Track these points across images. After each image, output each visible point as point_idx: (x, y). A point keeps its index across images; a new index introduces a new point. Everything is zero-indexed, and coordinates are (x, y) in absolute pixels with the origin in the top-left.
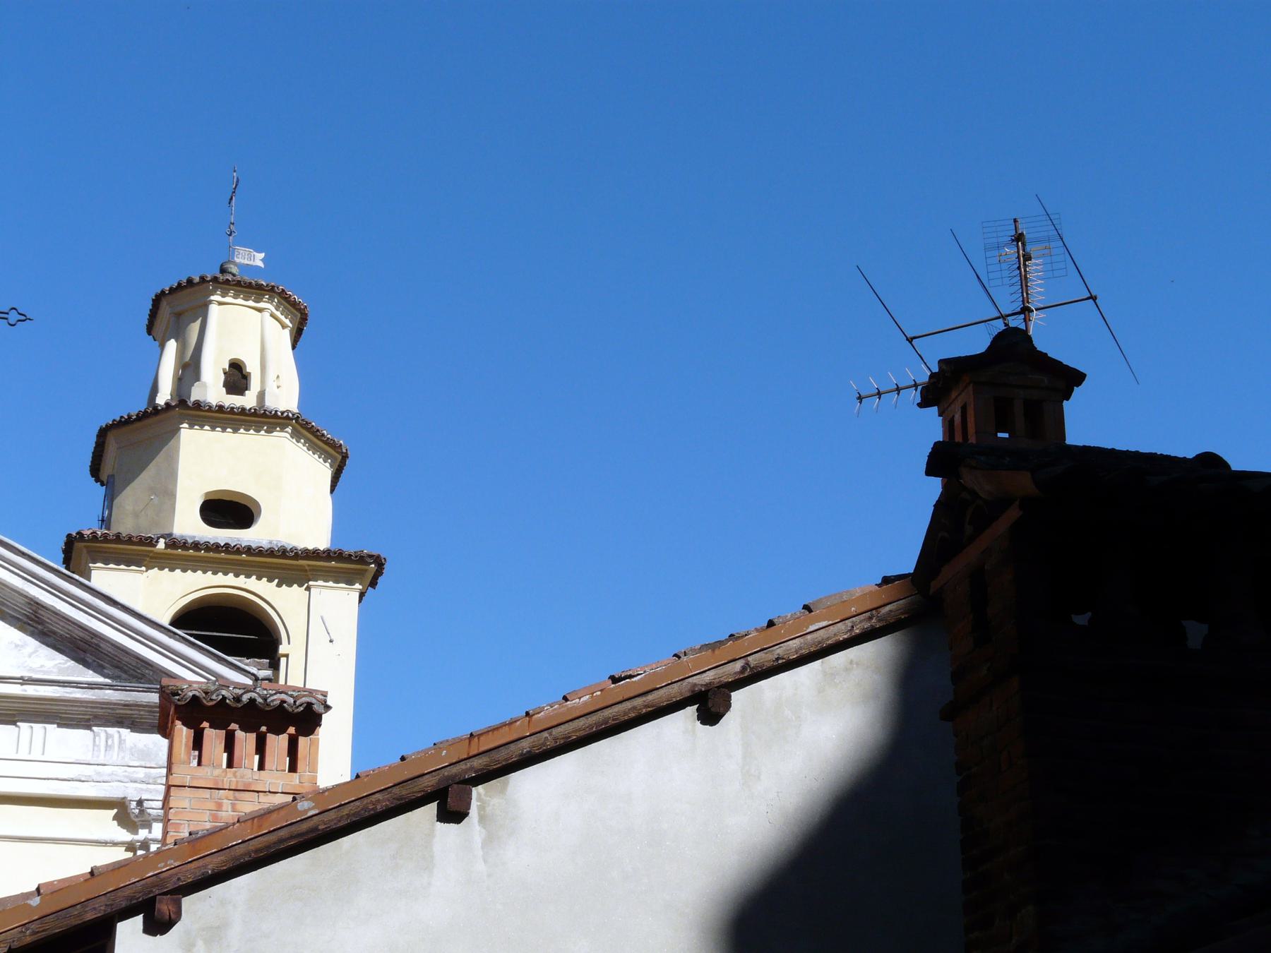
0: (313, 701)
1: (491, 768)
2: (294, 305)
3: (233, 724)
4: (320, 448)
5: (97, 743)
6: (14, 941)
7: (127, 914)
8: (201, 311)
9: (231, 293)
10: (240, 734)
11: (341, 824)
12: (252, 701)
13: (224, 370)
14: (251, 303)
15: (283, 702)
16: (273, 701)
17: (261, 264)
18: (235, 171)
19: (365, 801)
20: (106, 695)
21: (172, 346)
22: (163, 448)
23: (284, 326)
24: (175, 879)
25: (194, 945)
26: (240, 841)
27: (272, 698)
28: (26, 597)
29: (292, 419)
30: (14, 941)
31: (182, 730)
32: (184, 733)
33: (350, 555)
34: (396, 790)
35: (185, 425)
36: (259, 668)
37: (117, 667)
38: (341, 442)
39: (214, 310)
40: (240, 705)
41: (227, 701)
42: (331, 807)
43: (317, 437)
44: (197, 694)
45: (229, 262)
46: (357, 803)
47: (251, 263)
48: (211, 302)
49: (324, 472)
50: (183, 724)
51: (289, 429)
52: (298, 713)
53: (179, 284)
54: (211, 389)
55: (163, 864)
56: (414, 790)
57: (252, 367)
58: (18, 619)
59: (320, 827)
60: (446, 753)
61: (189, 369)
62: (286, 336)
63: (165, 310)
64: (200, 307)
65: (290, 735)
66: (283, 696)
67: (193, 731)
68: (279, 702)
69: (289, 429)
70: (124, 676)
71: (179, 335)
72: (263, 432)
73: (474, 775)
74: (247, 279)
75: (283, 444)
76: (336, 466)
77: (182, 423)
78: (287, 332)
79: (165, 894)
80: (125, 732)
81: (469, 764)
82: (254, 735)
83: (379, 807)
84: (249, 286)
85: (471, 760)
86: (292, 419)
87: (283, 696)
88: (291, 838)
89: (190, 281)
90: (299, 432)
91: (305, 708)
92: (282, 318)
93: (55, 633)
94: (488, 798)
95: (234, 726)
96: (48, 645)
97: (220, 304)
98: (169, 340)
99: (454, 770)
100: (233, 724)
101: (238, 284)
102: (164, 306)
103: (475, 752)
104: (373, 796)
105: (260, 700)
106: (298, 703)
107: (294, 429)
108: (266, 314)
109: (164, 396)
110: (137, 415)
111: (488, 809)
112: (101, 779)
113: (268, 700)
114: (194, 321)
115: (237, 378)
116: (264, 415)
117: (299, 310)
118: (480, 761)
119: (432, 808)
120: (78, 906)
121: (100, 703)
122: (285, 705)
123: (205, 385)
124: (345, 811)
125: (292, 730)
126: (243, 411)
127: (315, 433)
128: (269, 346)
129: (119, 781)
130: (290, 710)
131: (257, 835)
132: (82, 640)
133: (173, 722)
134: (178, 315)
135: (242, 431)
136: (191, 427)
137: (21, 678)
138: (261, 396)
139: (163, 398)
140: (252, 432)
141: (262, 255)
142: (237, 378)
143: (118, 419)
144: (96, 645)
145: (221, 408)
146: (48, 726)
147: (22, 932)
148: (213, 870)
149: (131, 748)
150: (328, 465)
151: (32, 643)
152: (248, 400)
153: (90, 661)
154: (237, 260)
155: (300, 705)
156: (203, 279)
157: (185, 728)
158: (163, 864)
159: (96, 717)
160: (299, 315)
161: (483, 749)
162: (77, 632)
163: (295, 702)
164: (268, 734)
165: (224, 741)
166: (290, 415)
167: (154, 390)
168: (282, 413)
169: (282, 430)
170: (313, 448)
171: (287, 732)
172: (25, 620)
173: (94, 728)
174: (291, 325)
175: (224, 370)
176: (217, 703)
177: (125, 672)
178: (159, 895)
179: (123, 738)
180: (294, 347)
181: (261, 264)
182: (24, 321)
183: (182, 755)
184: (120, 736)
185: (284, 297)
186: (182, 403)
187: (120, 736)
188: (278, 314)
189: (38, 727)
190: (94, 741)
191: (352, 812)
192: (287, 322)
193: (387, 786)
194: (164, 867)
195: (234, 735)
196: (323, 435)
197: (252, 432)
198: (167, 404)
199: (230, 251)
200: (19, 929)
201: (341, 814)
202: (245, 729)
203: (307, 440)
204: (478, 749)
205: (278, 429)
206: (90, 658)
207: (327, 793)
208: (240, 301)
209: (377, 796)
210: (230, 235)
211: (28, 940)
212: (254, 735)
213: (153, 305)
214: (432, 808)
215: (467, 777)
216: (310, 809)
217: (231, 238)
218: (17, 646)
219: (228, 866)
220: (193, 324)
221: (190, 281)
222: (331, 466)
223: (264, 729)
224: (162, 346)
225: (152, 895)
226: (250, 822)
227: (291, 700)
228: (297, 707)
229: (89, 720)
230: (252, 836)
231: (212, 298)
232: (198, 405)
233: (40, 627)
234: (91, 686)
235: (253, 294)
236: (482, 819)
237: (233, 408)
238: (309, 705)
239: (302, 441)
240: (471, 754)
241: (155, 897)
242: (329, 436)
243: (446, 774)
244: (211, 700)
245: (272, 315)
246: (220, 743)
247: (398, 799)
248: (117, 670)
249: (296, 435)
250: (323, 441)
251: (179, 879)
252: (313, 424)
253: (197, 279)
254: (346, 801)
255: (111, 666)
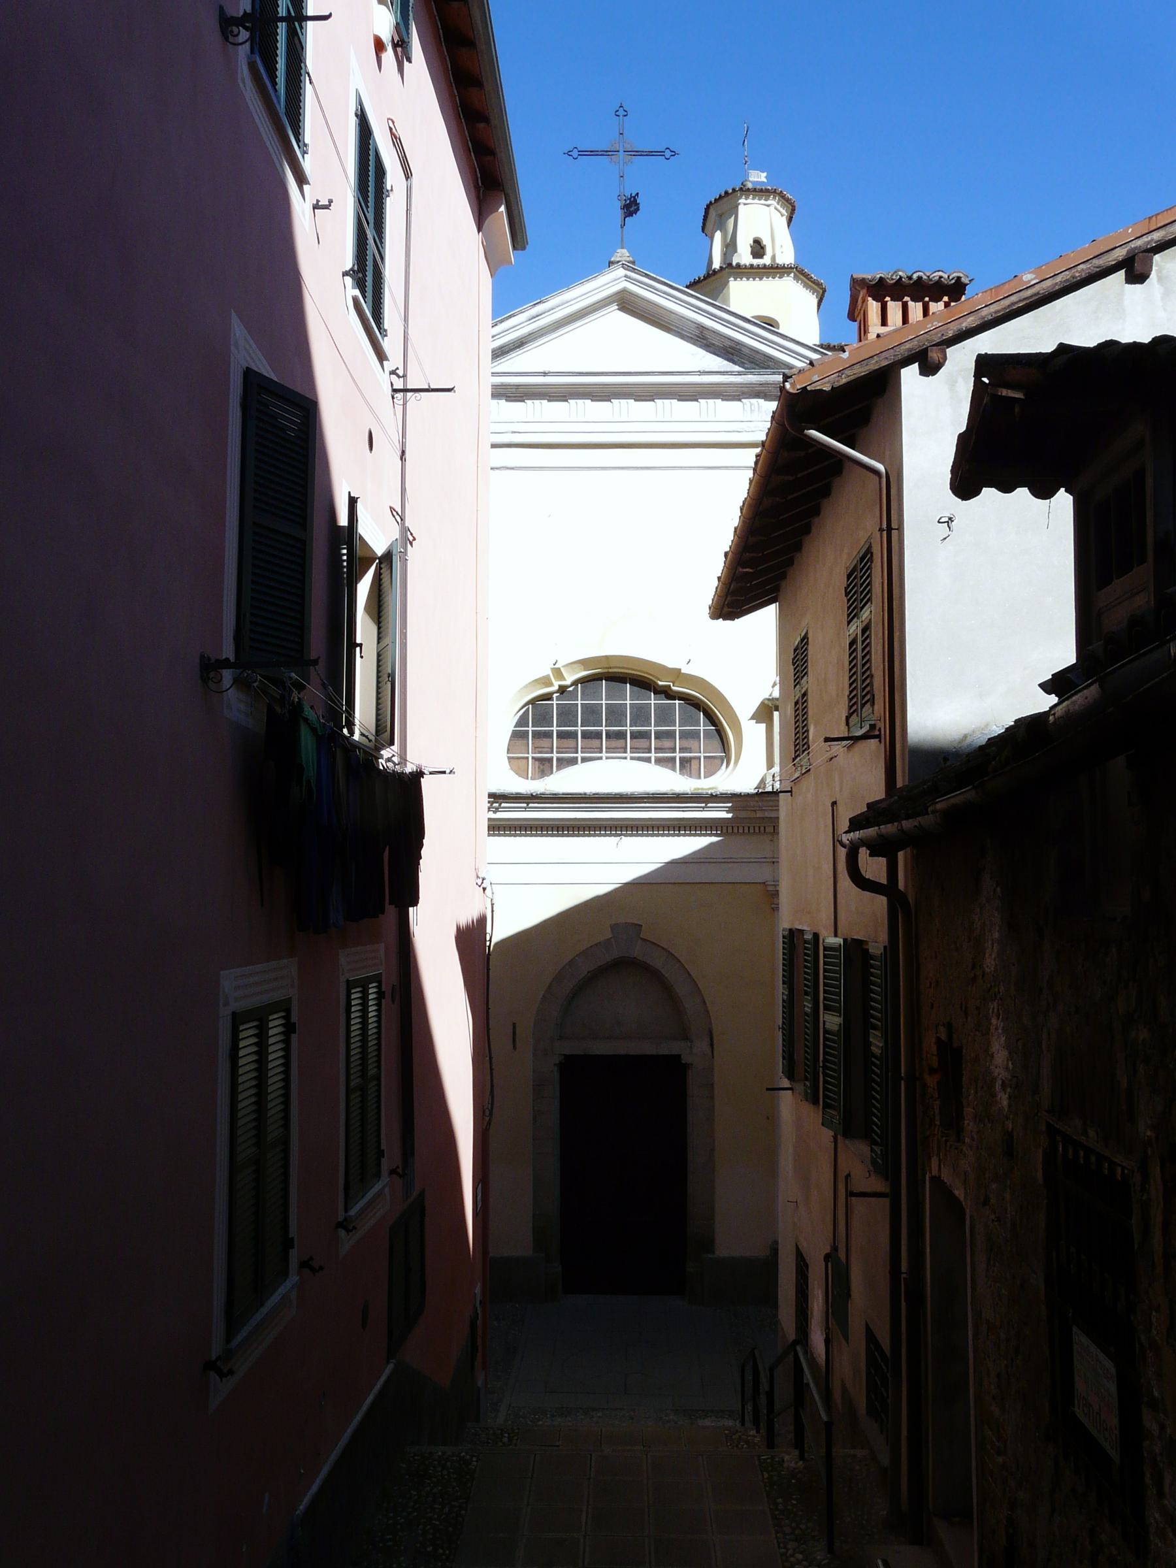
0: (961, 275)
1: (1167, 239)
2: (788, 200)
3: (906, 298)
4: (810, 286)
5: (745, 409)
6: (834, 382)
7: (906, 362)
8: (734, 210)
9: (751, 197)
10: (911, 304)
11: (1057, 288)
12: (920, 278)
13: (750, 244)
14: (763, 202)
15: (941, 277)
16: (934, 277)
17: (765, 180)
18: (745, 123)
19: (1074, 270)
20: (749, 378)
21: (718, 235)
22: (719, 295)
23: (782, 215)
24: (940, 335)
25: (956, 382)
26: (983, 306)
27: (933, 275)
28: (695, 323)
29: (793, 268)
30: (834, 382)
31: (873, 304)
32: (874, 306)
33: (835, 346)
34: (1094, 261)
35: (732, 279)
36: (766, 444)
37: (752, 362)
38: (822, 281)
39: (741, 208)
40: (912, 282)
41: (903, 279)
42: (1048, 277)
43: (808, 279)
44: (883, 276)
45: (746, 180)
46: (1067, 273)
47: (759, 180)
48: (739, 204)
49: (813, 300)
50: (874, 300)
51: (792, 275)
52: (952, 284)
53: (720, 195)
54: (744, 256)
55: (930, 325)
56: (1109, 260)
57: (766, 242)
58: (691, 338)
59: (1041, 292)
60: (1132, 231)
61: (730, 247)
62: (784, 221)
63: (713, 213)
64: (734, 208)
65: (945, 302)
66: (941, 274)
67: (880, 304)
68: (938, 277)
69: (792, 275)
70: (757, 367)
71: (721, 226)
72: (777, 278)
73: (1154, 245)
74: (758, 187)
75: (789, 286)
76: (819, 297)
77: (730, 278)
78: (784, 218)
79: (934, 345)
80: (761, 401)
81: (1149, 237)
82: (921, 304)
83: (1083, 274)
84: (761, 191)
85: (1152, 234)
86: (793, 268)
87: (941, 274)
88: (1020, 301)
89: (726, 193)
90: (798, 277)
91: (956, 281)
92: (781, 209)
93: (714, 344)
94: (1163, 264)
95: (906, 299)
96: (711, 353)
97: (745, 204)
98: (716, 231)
99: (1139, 243)
100: (906, 298)
101: (755, 190)
102: (712, 212)
103: (1155, 227)
104: (1079, 267)
105: (925, 277)
106: (951, 278)
107: (795, 275)
108: (772, 208)
109: (716, 265)
110: (704, 277)
111: (1164, 272)
112: (750, 430)
113: (931, 277)
114: (730, 218)
115: (758, 248)
116: (777, 268)
117: (790, 204)
118: (1158, 234)
119: (1121, 274)
120: (875, 357)
121: (746, 384)
122: (942, 279)
123: (740, 255)
124: (1059, 279)
125: (946, 299)
126: (765, 267)
127: (807, 276)
128: (774, 227)
129: (761, 431)
130: (946, 282)
131: (995, 300)
132: (731, 347)
133: (864, 301)
134: (721, 216)
135: (765, 279)
136: (735, 280)
137: (699, 372)
138: (774, 258)
139: (716, 265)
140: (770, 278)
141: (765, 174)
142: (758, 248)
143: (693, 281)
144: (740, 350)
145: (752, 266)
146: (716, 401)
147: (839, 376)
148: (966, 327)
149: (765, 411)
150: (815, 296)
151: (701, 352)
152: (766, 260)
153: (735, 360)
154: (751, 179)
155: (952, 279)
156: (734, 190)
157: (874, 302)
158: (930, 325)
159: (743, 393)
160: (791, 207)
161: (1159, 225)
162: (727, 343)
163: (949, 277)
164: (930, 303)
165: (901, 309)
166: (793, 266)
167: (710, 262)
168: (788, 265)
169: (788, 276)
170: (806, 286)
171: (943, 300)
172: (696, 338)
173: (743, 400)
174: (786, 214)
175: (750, 244)
176: (896, 281)
177: (757, 365)
178: (931, 346)
179: (760, 405)
180: (788, 226)
181: (765, 180)
182: (674, 155)
183: (875, 320)
184: (758, 404)
185: (782, 196)
186: (730, 265)
187: (758, 404)
188: (779, 207)
189: (711, 401)
190: (744, 408)
191: (1064, 279)
192: (784, 212)
193: (1089, 258)
194: (932, 327)
195: (907, 304)
196: (811, 277)
197: (770, 278)
198: (721, 267)
199: (747, 175)
200: (837, 374)
201: (1054, 282)
202: (914, 300)
203: (803, 282)
204: (1156, 224)
205: (786, 275)
206: (736, 359)
207: (1043, 267)
208: (756, 201)
209: (1081, 266)
210: (745, 164)
211: (844, 381)
212: (921, 304)
213: (705, 212)
214: (1121, 274)
215: (1149, 247)
216: (1032, 280)
217: (746, 165)
218: (693, 355)
219: (976, 324)
220: (729, 220)
221: (726, 193)
222: (817, 297)
223: (927, 299)
224: (712, 238)
225: (925, 347)
226: (989, 292)
227: (946, 276)
228: (950, 281)
229: (739, 395)
230: (993, 301)
231: (740, 201)
232: (738, 265)
233: (705, 342)
234: (739, 374)
235: (763, 195)
236: (1160, 279)
237: (759, 265)
238: (959, 278)
239: (800, 282)
240: (1151, 229)
241: (927, 348)
242: (815, 278)
243: (1133, 246)
244: (893, 279)
245: (776, 209)
246: (899, 310)
247: (1098, 267)
248: (753, 365)
249: (796, 278)
250: (812, 282)
251: (943, 335)
252: (806, 270)
253: (730, 191)
254: (1059, 272)
255: (750, 362)
